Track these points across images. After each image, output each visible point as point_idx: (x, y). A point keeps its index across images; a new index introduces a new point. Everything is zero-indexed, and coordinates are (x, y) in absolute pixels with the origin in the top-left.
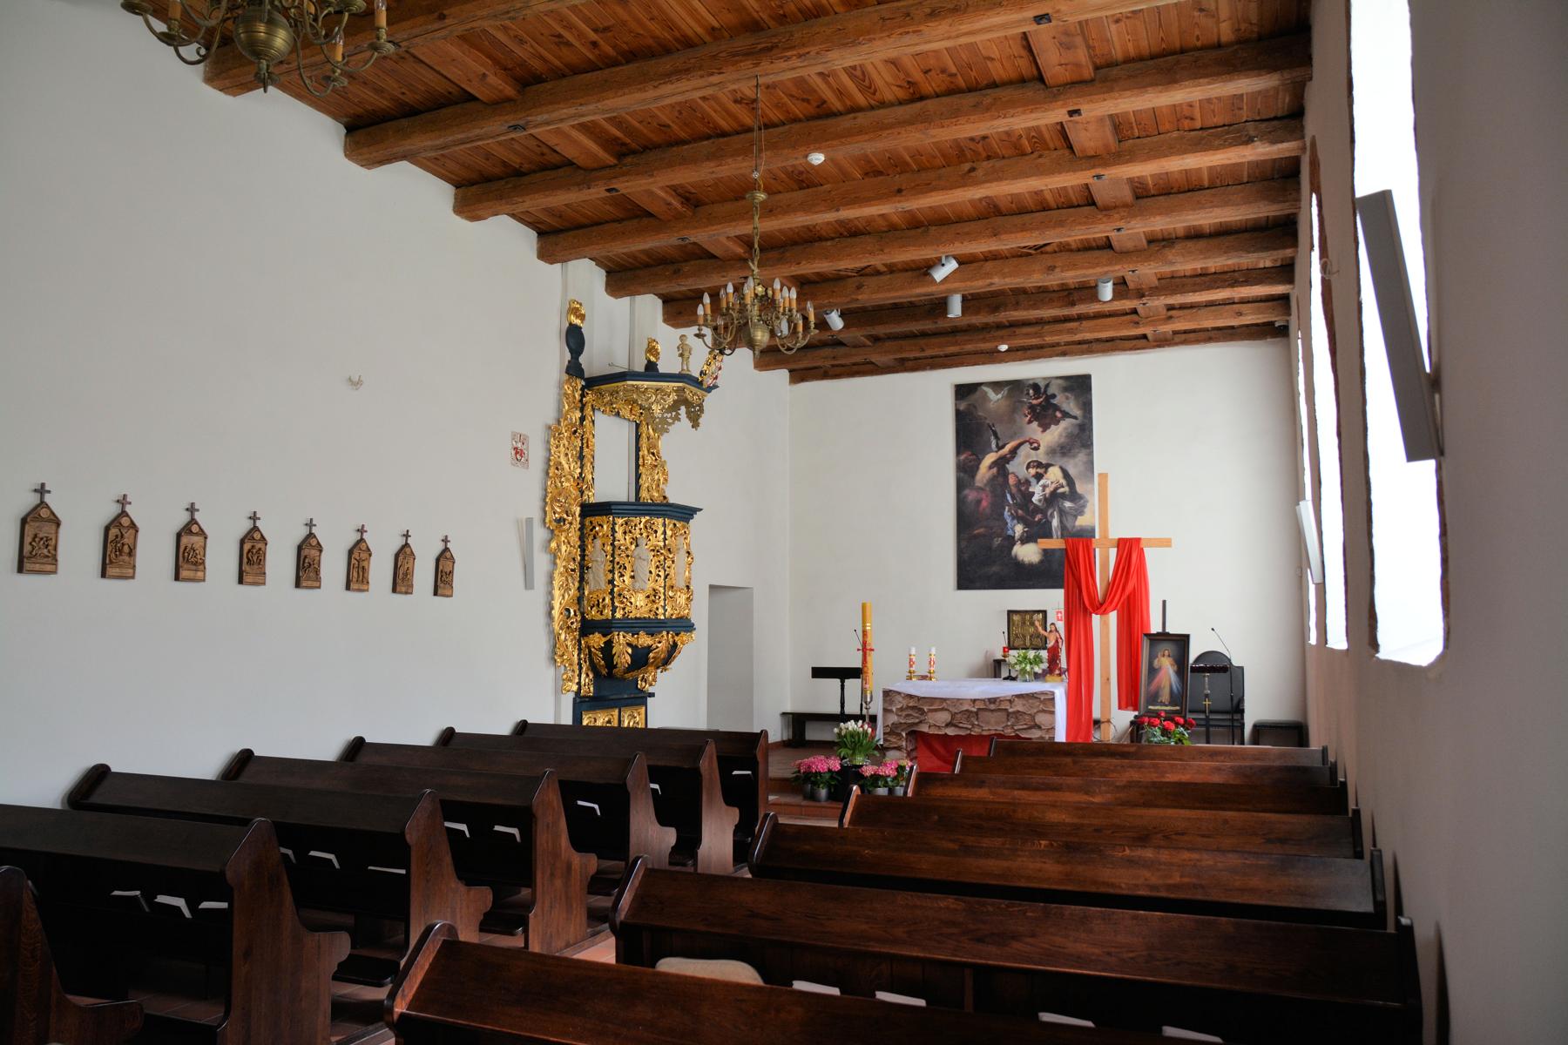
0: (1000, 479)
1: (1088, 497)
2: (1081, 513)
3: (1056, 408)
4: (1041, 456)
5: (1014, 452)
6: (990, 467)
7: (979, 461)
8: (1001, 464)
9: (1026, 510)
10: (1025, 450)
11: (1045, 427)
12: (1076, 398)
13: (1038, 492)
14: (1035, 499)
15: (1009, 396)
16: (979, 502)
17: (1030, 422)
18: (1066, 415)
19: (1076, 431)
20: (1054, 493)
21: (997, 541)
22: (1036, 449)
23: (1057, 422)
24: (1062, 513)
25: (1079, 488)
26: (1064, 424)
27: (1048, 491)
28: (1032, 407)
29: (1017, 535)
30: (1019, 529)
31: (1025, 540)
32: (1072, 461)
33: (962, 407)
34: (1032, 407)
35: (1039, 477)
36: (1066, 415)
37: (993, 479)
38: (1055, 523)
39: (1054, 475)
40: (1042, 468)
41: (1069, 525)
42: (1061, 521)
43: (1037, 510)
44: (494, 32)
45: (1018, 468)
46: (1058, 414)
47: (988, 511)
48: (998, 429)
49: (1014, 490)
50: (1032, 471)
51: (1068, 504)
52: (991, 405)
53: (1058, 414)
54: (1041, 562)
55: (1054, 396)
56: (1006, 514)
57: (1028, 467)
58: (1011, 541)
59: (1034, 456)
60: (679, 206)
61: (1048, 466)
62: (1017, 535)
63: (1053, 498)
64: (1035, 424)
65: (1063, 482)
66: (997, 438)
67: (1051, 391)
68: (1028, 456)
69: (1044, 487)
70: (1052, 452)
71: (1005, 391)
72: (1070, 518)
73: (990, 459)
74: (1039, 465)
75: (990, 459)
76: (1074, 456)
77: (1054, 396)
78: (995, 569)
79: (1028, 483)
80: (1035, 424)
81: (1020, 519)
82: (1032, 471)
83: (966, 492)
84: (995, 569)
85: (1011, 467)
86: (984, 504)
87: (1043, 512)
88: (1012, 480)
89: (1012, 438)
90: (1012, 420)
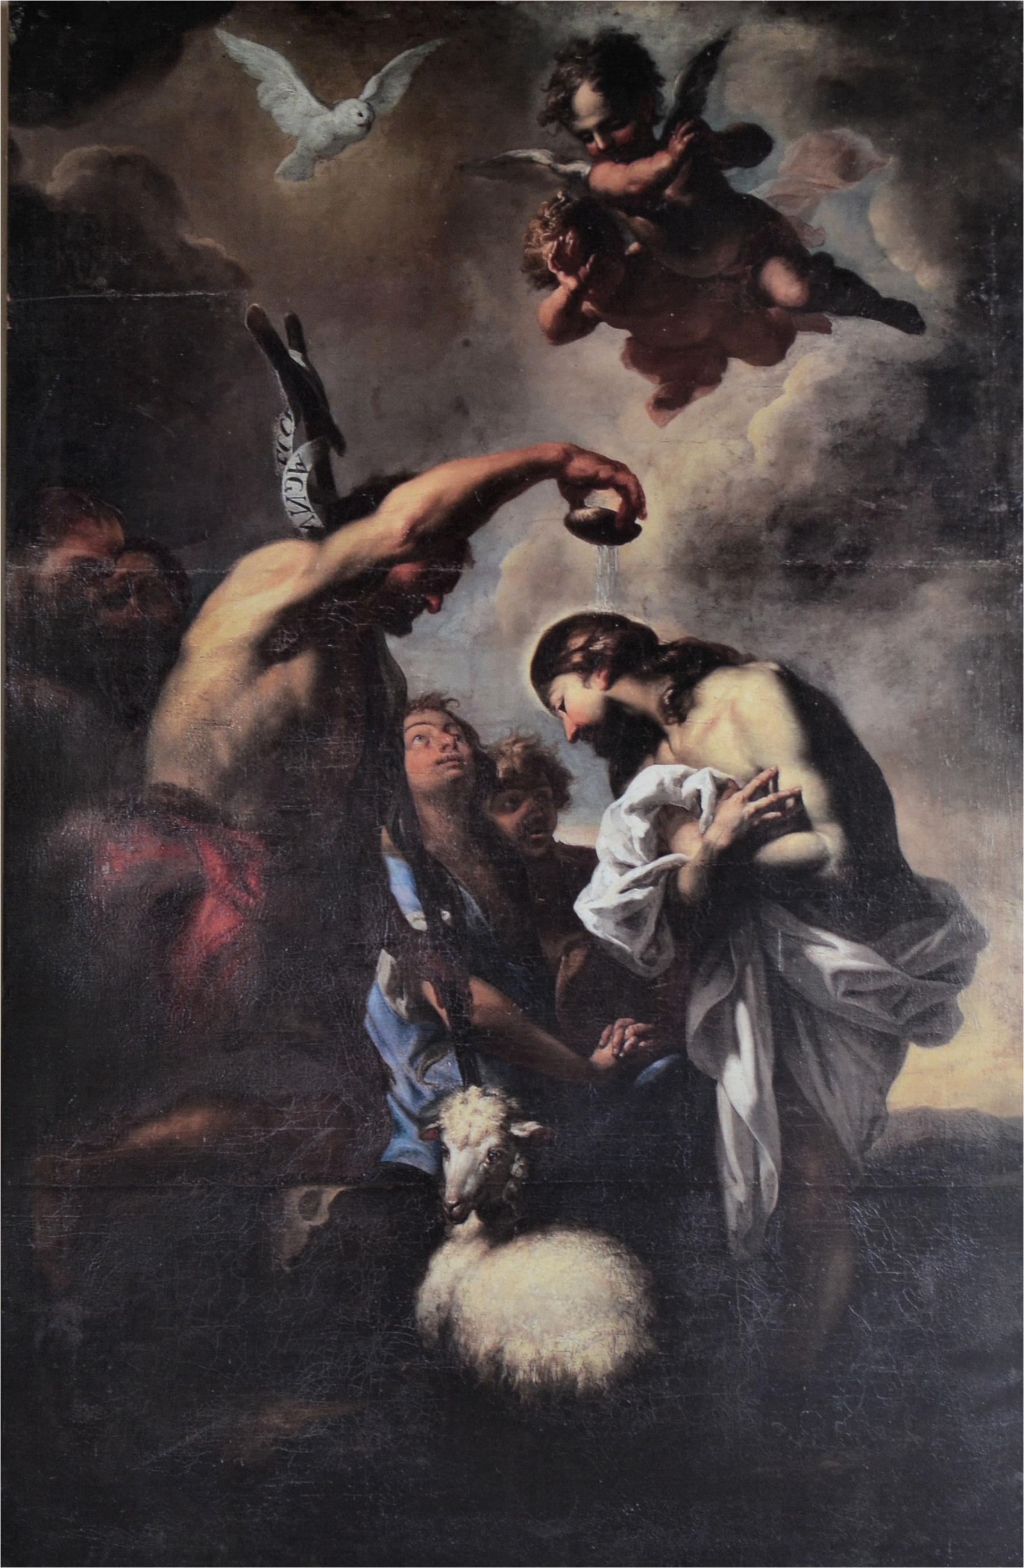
0: (340, 746)
1: (980, 904)
2: (934, 1023)
3: (770, 233)
4: (644, 583)
5: (446, 544)
6: (266, 650)
7: (184, 602)
8: (349, 627)
9: (529, 987)
10: (530, 531)
11: (681, 374)
12: (918, 169)
13: (615, 856)
14: (596, 904)
15: (411, 124)
16: (173, 907)
17: (570, 326)
18: (838, 291)
19: (908, 418)
20: (734, 862)
21: (306, 1213)
22: (614, 530)
23: (771, 345)
24: (793, 1015)
25: (922, 837)
26: (817, 358)
27: (690, 846)
28: (590, 219)
29: (459, 1167)
30: (472, 1123)
31: (512, 1209)
32: (871, 639)
33: (62, 174)
34: (590, 219)
35: (625, 741)
36: (838, 291)
37: (283, 739)
38: (740, 1084)
39: (739, 726)
40: (650, 676)
41: (839, 1106)
42: (783, 1081)
43: (608, 982)
44: (923, 943)
45: (473, 663)
46: (782, 284)
47: (244, 980)
48: (334, 364)
49: (440, 827)
50: (580, 695)
51: (834, 954)
52: (284, 180)
53: (782, 284)
54: (633, 1373)
55: (752, 144)
56: (380, 1006)
57: (547, 667)
58: (412, 1214)
59: (595, 582)
60: (512, 153)
61: (690, 665)
62: (459, 1167)
63: (727, 905)
64: (606, 347)
65: (798, 780)
66: (322, 430)
67: (731, 103)
68: (549, 578)
69: (666, 816)
70: (725, 556)
71: (392, 81)
72: (847, 1059)
73: (263, 584)
74: (628, 649)
75: (263, 584)
76: (887, 603)
77: (752, 144)
78: (286, 1418)
79: (544, 782)
80: (606, 347)
81: (481, 1054)
82: (580, 695)
83: (82, 826)
84: (286, 1418)
85: (427, 656)
86: (216, 922)
87: (655, 1002)
88: (425, 757)
89: (435, 436)
90: (434, 306)
